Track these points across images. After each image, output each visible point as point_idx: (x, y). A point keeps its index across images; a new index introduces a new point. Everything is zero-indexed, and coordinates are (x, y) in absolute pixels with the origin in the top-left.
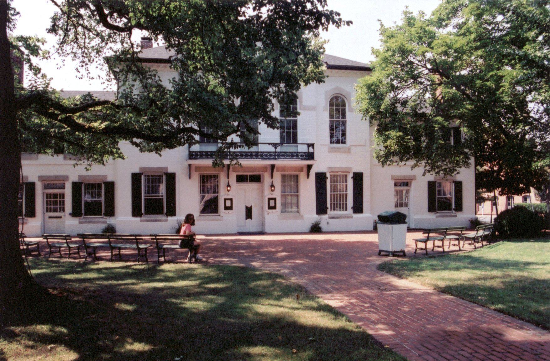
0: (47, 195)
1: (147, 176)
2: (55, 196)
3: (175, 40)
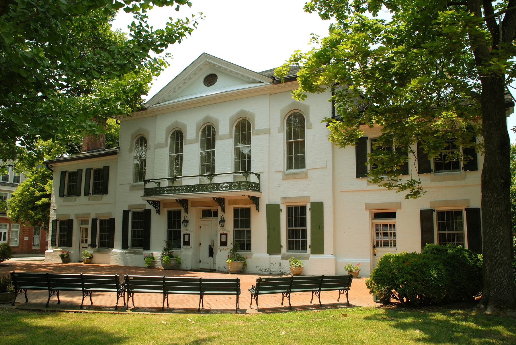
0: (377, 226)
1: (134, 213)
2: (385, 227)
3: (41, 107)
